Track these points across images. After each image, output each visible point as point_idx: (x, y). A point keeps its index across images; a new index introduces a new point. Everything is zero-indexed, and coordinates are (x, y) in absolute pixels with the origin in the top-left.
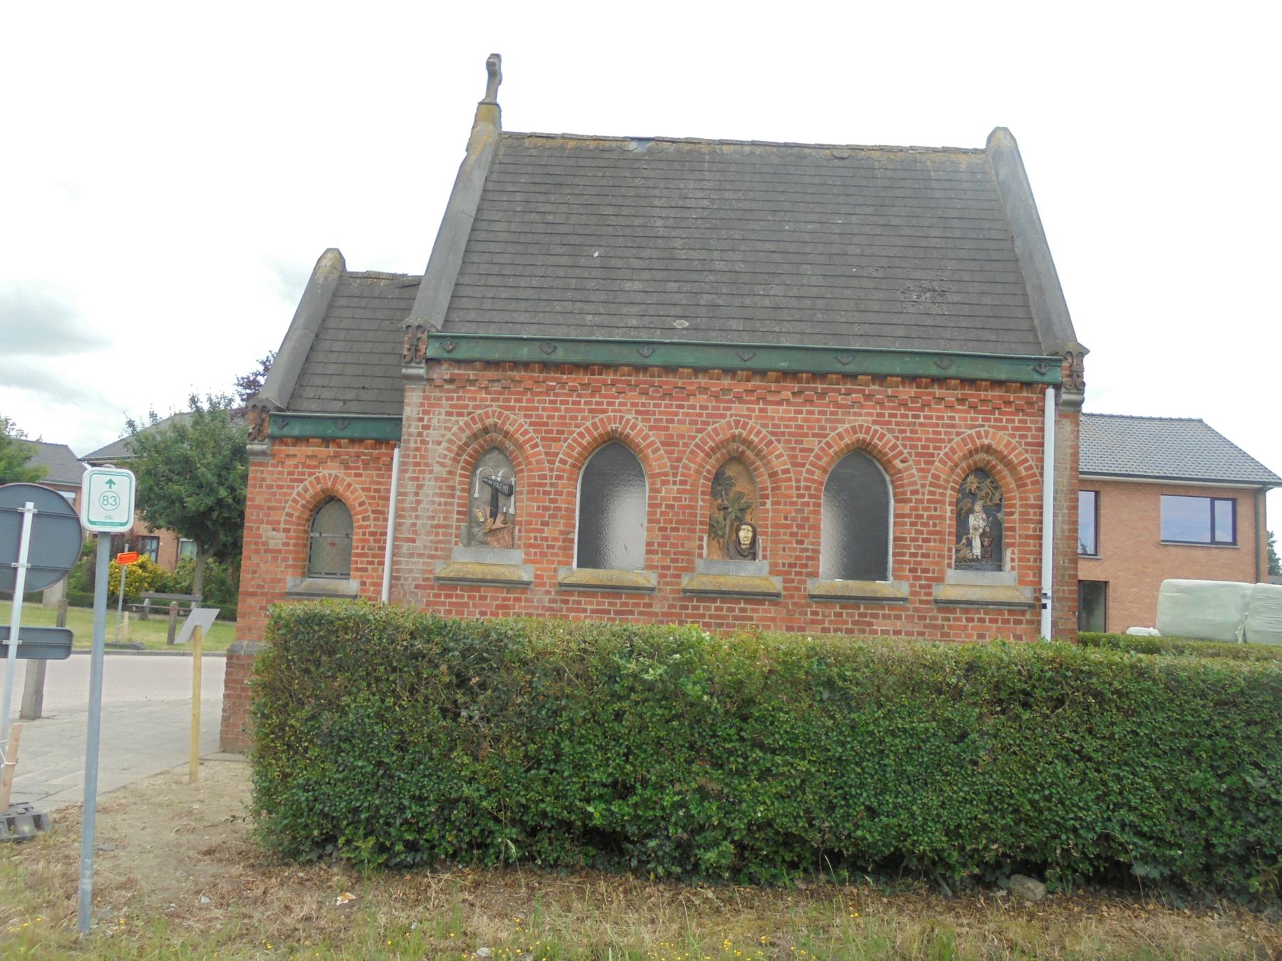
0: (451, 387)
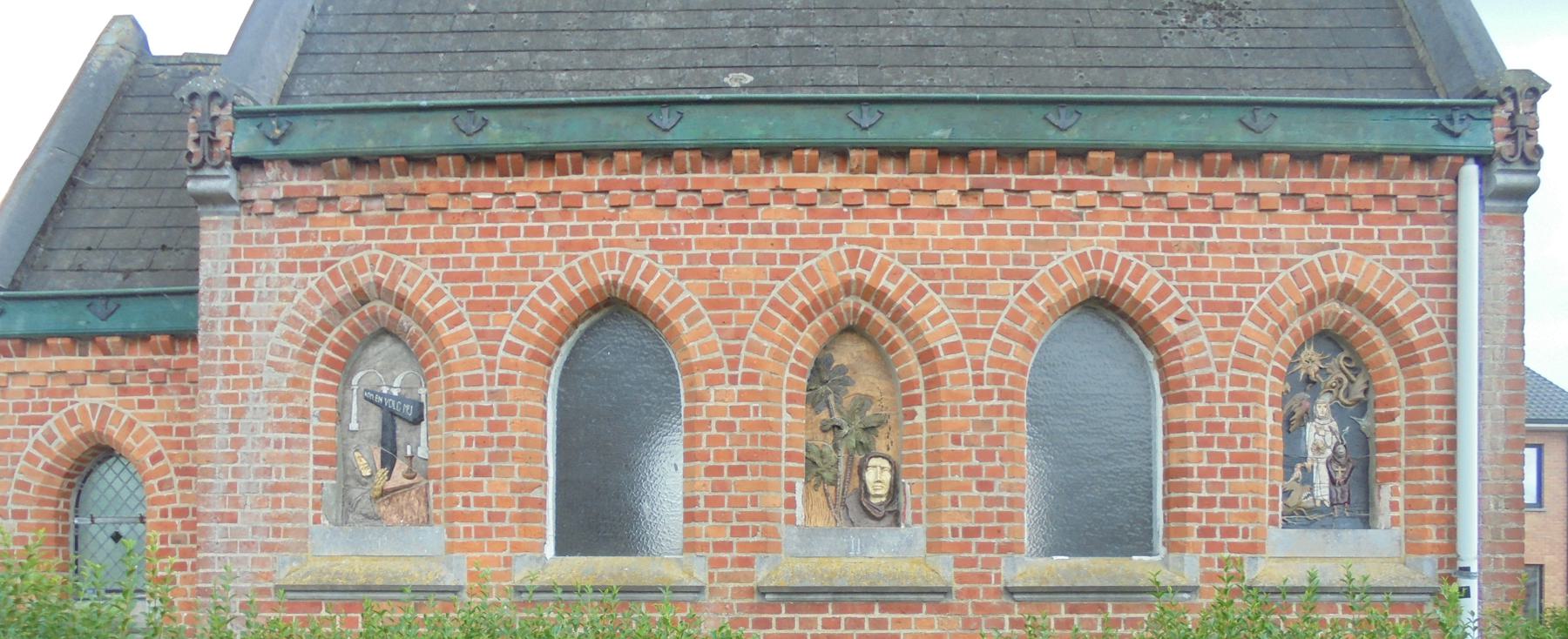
0: (291, 214)
